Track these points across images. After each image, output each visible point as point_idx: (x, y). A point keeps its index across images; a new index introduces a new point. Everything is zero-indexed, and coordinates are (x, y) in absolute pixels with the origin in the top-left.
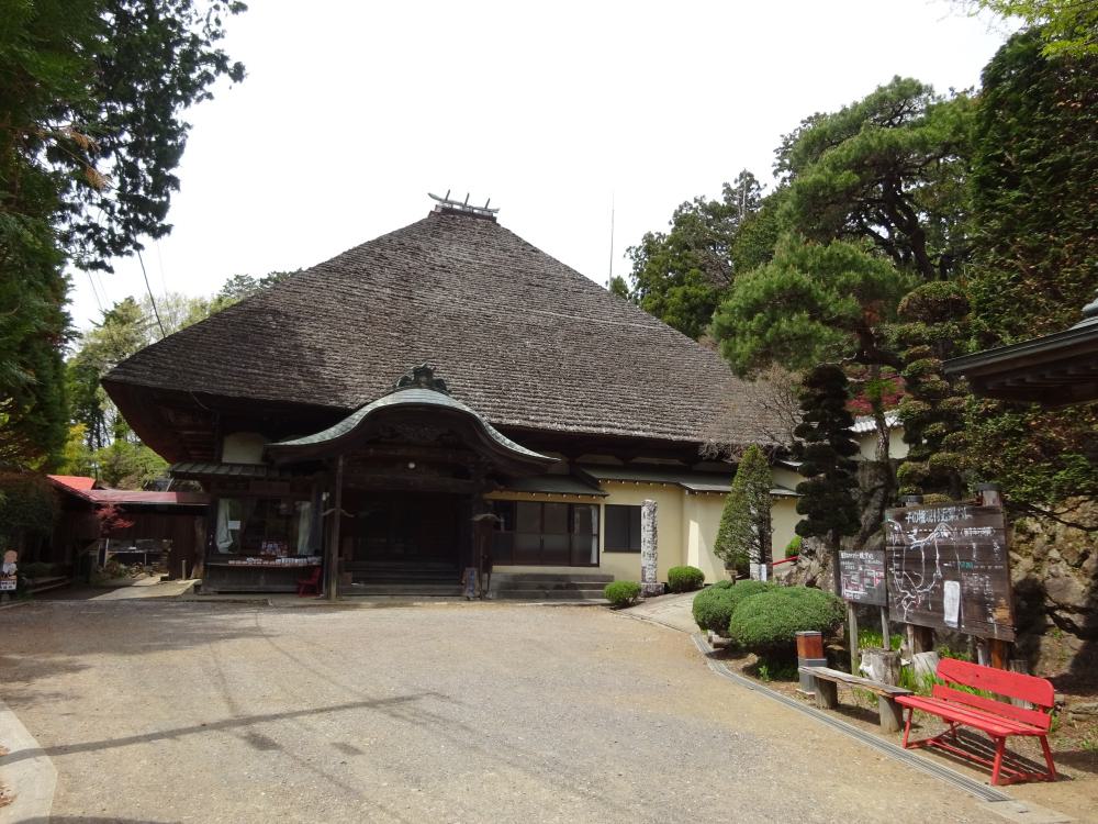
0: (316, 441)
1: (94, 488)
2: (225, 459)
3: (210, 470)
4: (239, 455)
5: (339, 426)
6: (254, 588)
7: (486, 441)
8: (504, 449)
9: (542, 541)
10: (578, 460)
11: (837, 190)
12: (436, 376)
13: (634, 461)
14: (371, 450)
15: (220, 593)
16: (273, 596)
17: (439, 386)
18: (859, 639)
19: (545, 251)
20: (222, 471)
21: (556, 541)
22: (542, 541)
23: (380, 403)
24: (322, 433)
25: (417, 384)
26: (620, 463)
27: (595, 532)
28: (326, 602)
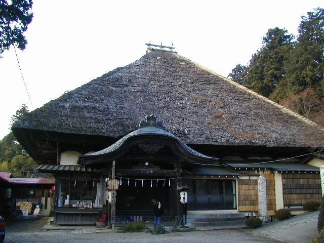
0: (108, 152)
1: (11, 177)
2: (62, 163)
3: (56, 168)
4: (68, 161)
5: (113, 146)
6: (77, 223)
7: (182, 151)
8: (192, 155)
9: (209, 198)
10: (223, 159)
11: (16, 44)
12: (159, 120)
13: (249, 158)
14: (128, 157)
15: (61, 225)
16: (85, 226)
17: (159, 125)
18: (168, 232)
19: (133, 61)
20: (61, 169)
21: (215, 198)
22: (209, 198)
23: (131, 134)
24: (105, 150)
25: (147, 125)
26: (243, 160)
27: (234, 193)
28: (109, 230)
